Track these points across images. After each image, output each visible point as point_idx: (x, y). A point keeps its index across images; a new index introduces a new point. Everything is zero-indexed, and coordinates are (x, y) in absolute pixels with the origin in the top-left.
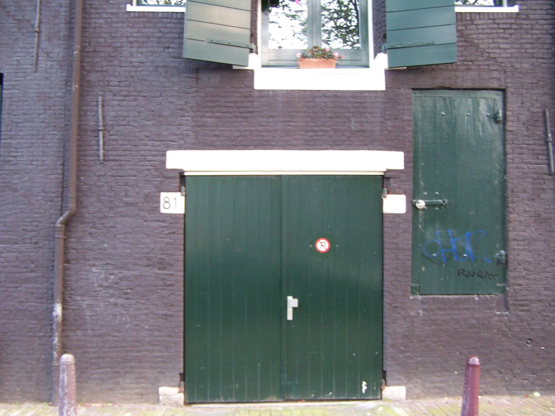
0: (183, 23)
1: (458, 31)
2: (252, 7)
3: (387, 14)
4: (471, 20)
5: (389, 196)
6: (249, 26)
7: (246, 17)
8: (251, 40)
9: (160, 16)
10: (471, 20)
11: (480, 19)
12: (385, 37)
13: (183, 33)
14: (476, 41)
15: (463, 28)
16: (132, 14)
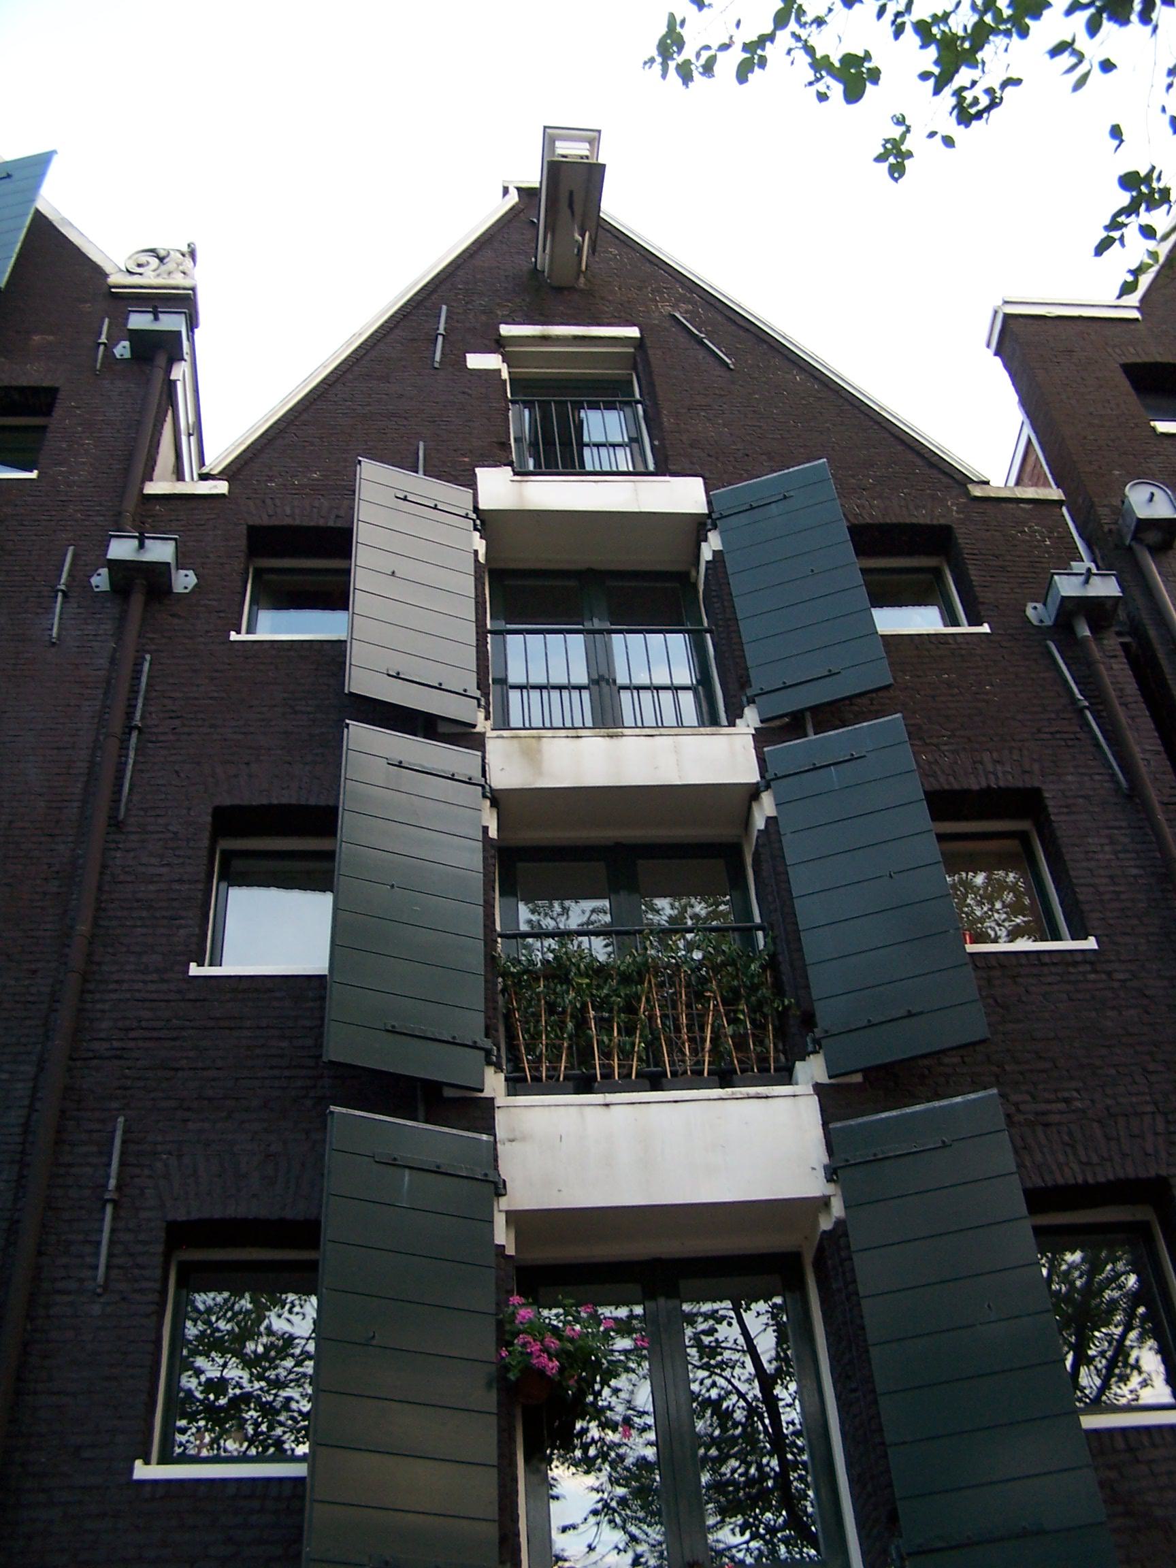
0: (301, 1511)
1: (1102, 1484)
2: (501, 1456)
3: (863, 1302)
4: (1130, 1449)
5: (754, 781)
6: (493, 1511)
7: (486, 1485)
8: (501, 1553)
9: (231, 1490)
10: (1130, 1449)
11: (1154, 1445)
12: (893, 1517)
13: (298, 1539)
14: (1159, 1512)
15: (1113, 1474)
16: (148, 1488)
